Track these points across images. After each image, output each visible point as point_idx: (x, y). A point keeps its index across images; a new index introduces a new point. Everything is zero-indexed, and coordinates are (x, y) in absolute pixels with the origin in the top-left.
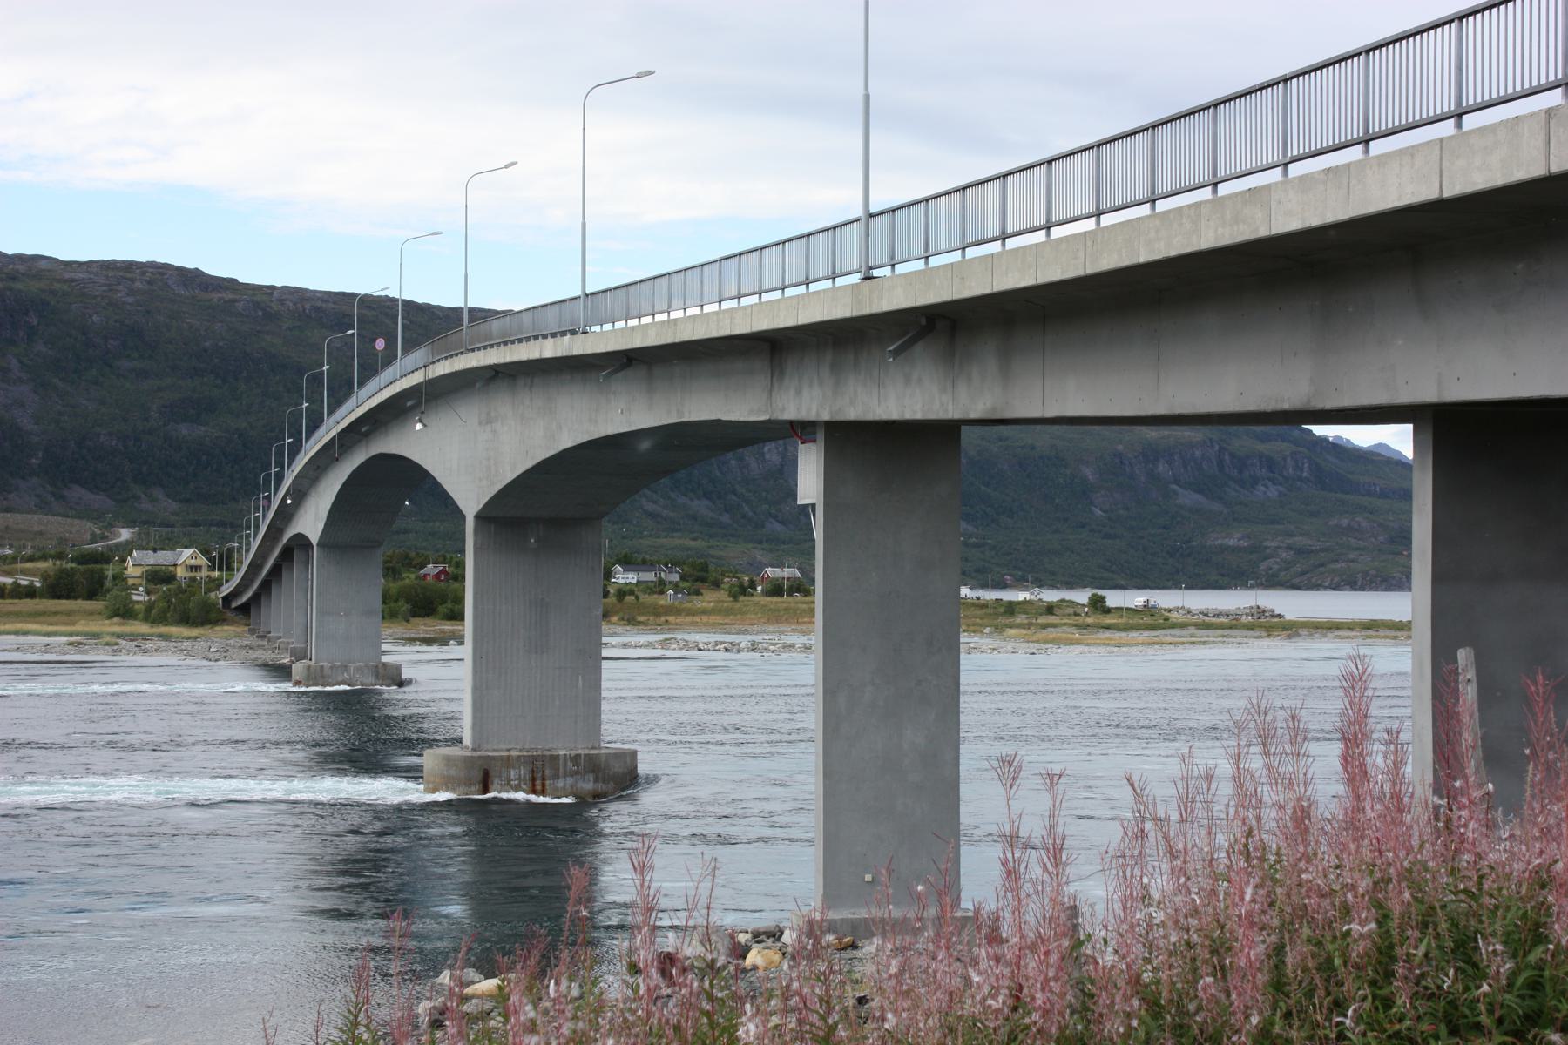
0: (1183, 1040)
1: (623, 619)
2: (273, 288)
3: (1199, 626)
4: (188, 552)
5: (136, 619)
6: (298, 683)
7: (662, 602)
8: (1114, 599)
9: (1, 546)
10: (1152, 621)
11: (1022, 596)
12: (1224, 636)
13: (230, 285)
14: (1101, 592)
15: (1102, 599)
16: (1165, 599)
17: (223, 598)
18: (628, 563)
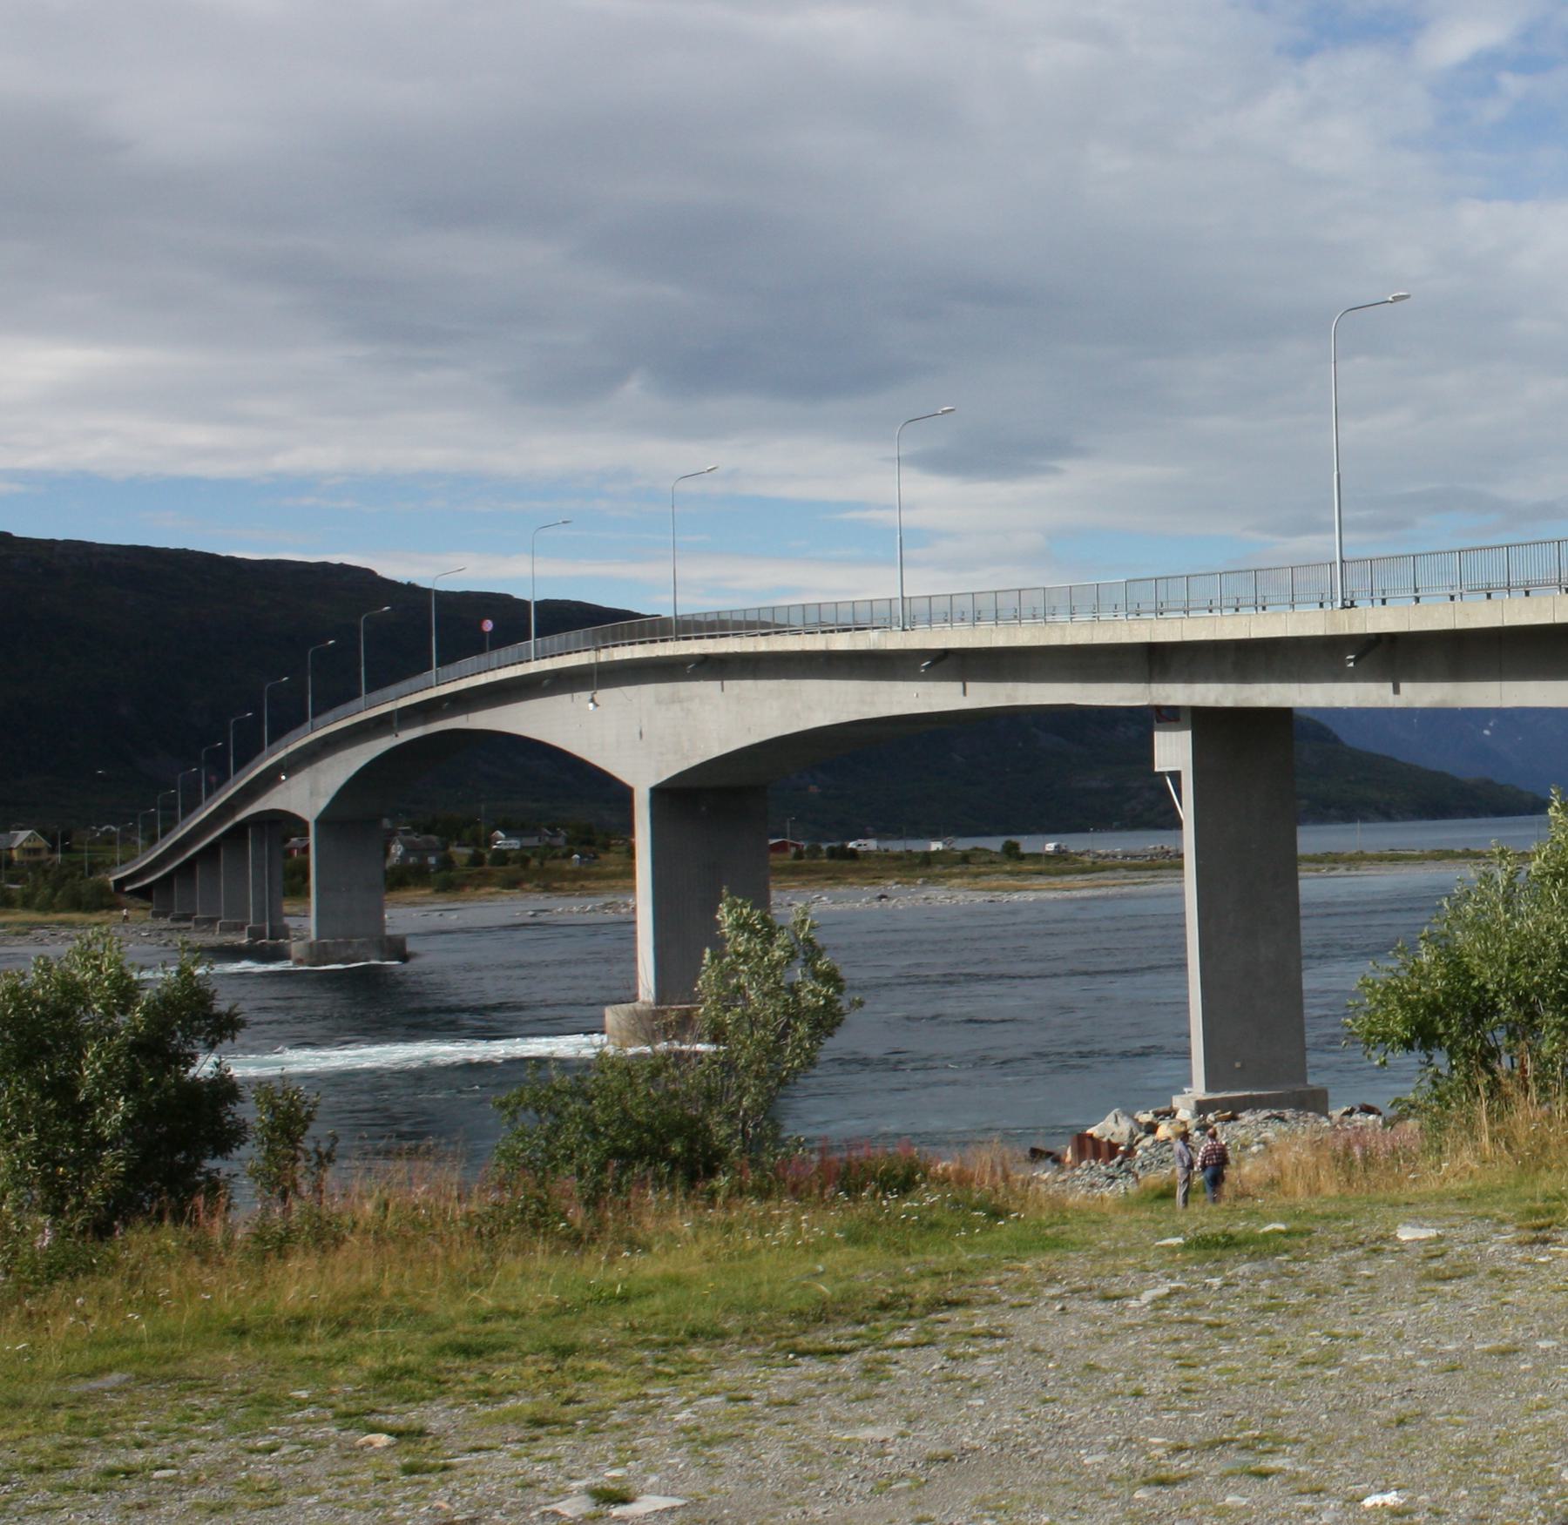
0: (1553, 1140)
1: (538, 886)
2: (53, 542)
3: (1129, 868)
4: (23, 835)
5: (13, 907)
6: (299, 962)
7: (568, 867)
8: (1027, 844)
9: (5, 826)
10: (1062, 863)
11: (936, 846)
12: (1155, 876)
13: (52, 544)
14: (1014, 839)
15: (1016, 846)
16: (1076, 843)
17: (115, 881)
18: (510, 830)
